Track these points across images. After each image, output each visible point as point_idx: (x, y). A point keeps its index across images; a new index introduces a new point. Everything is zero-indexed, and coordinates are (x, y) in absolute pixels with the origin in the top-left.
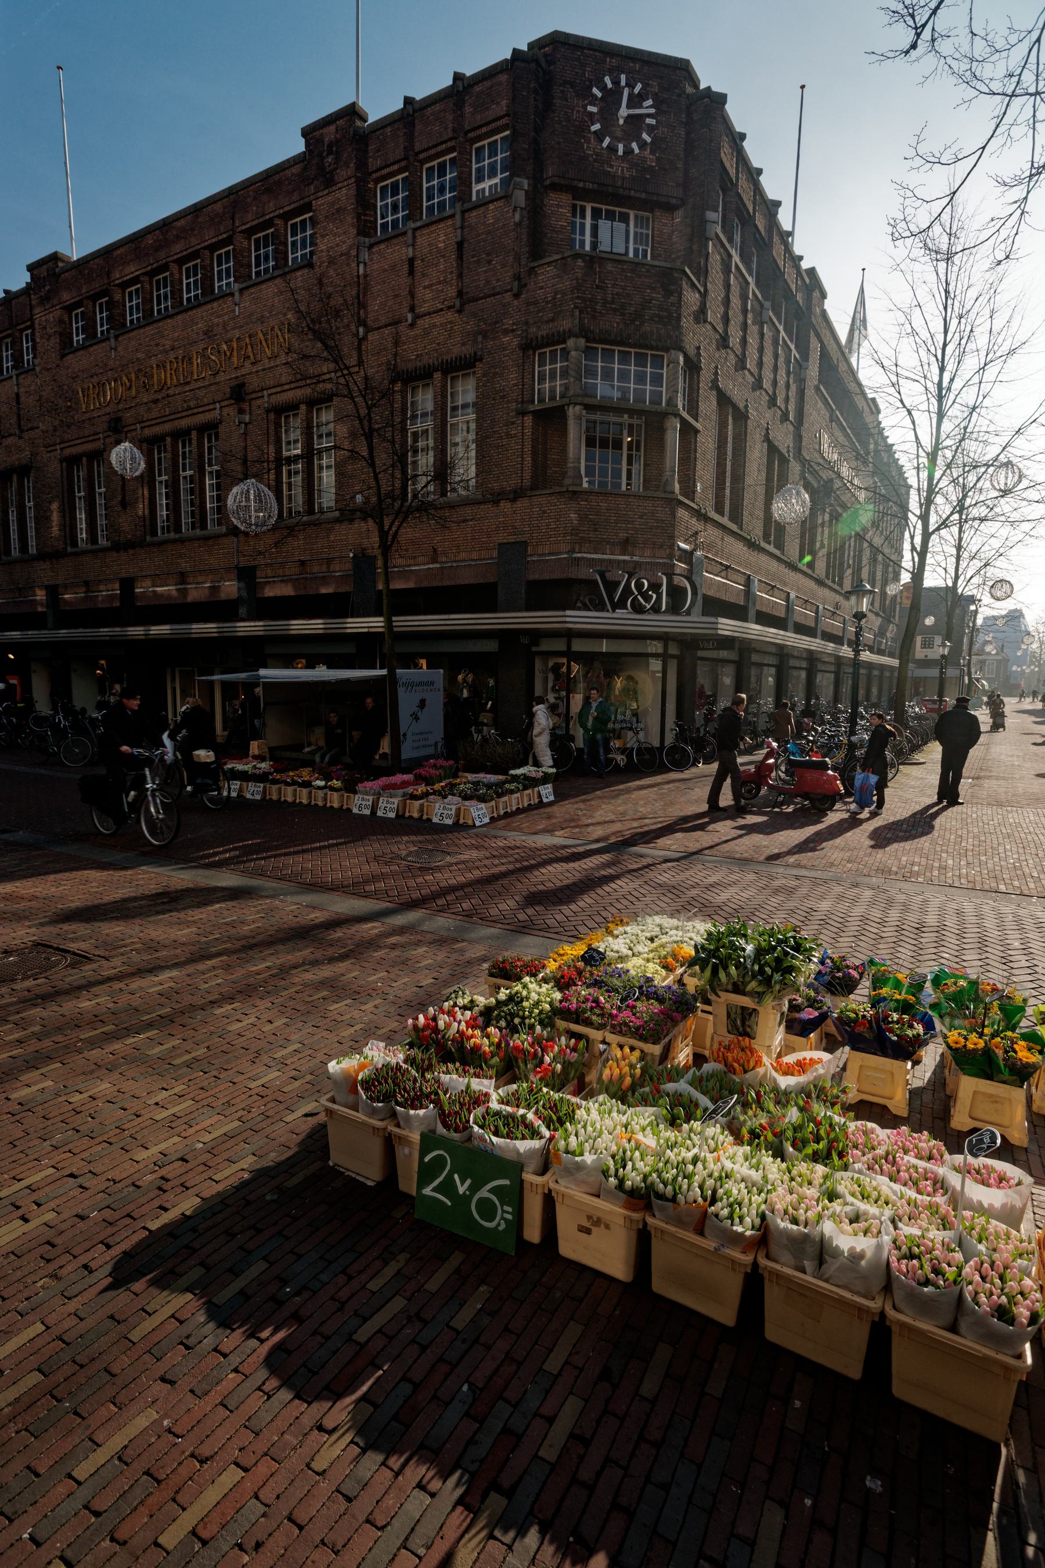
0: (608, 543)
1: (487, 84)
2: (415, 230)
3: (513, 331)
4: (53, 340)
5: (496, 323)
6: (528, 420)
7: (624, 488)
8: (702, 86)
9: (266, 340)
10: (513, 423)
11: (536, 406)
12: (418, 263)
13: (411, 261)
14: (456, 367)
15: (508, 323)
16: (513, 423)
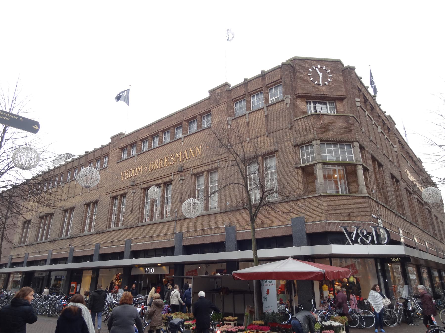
0: (341, 216)
1: (274, 72)
2: (249, 114)
3: (290, 140)
4: (115, 158)
5: (283, 138)
6: (300, 171)
7: (340, 193)
8: (345, 66)
9: (193, 151)
10: (293, 172)
11: (302, 165)
12: (250, 123)
13: (248, 123)
14: (271, 154)
15: (287, 138)
16: (293, 172)
